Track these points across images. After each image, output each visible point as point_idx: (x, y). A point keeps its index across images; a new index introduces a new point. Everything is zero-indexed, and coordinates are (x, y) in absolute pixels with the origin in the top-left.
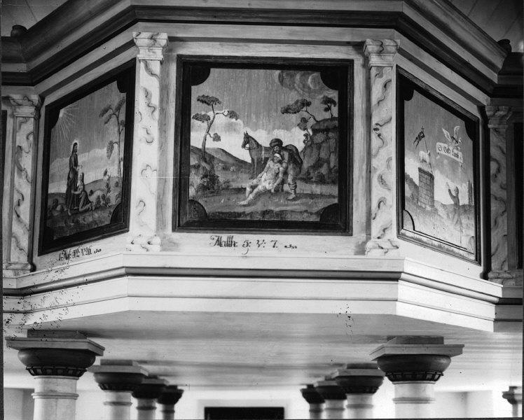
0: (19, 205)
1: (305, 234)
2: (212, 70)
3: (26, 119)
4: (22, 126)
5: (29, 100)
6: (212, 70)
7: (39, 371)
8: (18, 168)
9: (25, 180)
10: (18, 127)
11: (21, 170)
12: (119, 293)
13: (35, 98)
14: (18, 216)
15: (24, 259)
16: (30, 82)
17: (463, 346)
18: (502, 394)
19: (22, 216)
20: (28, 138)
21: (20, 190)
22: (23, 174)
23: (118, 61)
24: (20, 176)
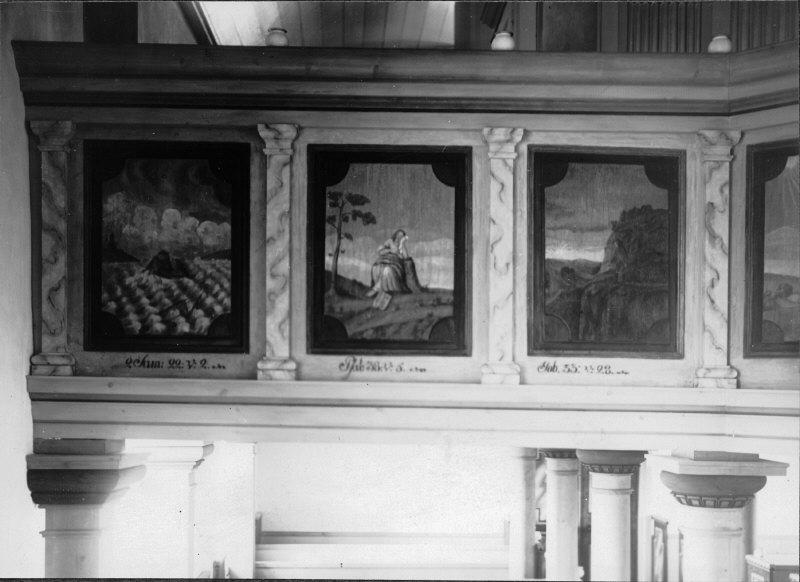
0: (713, 286)
1: (642, 357)
2: (452, 190)
3: (719, 164)
4: (714, 174)
5: (728, 139)
6: (452, 190)
7: (696, 502)
8: (710, 234)
9: (720, 252)
10: (707, 176)
11: (713, 237)
12: (728, 404)
13: (736, 135)
14: (713, 302)
15: (722, 360)
16: (726, 111)
17: (646, 452)
18: (219, 559)
19: (717, 302)
20: (722, 191)
21: (714, 264)
22: (716, 242)
23: (51, 184)
24: (713, 246)
